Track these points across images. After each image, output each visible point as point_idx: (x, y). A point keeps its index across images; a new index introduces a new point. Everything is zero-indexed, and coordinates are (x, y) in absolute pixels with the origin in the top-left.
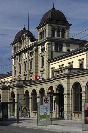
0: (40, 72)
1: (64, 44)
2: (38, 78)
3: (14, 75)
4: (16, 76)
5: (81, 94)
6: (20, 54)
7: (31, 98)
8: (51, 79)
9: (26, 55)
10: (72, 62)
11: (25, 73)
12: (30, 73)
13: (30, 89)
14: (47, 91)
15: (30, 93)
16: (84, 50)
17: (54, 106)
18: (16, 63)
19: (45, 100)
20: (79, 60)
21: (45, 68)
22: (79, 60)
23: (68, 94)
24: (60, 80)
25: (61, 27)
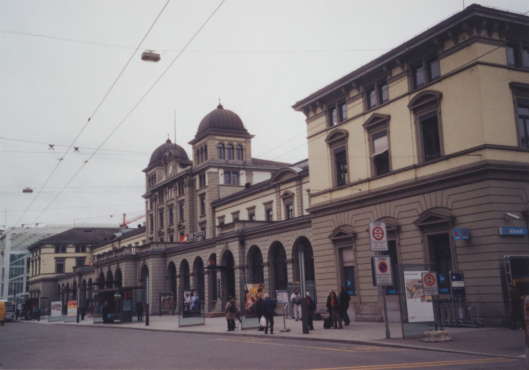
0: (198, 225)
1: (241, 172)
4: (154, 233)
5: (234, 270)
8: (209, 241)
9: (172, 194)
10: (254, 208)
11: (181, 223)
13: (177, 260)
14: (206, 263)
15: (178, 267)
16: (272, 186)
17: (219, 289)
18: (154, 208)
19: (427, 281)
20: (265, 204)
21: (208, 217)
22: (265, 204)
23: (242, 268)
25: (235, 141)
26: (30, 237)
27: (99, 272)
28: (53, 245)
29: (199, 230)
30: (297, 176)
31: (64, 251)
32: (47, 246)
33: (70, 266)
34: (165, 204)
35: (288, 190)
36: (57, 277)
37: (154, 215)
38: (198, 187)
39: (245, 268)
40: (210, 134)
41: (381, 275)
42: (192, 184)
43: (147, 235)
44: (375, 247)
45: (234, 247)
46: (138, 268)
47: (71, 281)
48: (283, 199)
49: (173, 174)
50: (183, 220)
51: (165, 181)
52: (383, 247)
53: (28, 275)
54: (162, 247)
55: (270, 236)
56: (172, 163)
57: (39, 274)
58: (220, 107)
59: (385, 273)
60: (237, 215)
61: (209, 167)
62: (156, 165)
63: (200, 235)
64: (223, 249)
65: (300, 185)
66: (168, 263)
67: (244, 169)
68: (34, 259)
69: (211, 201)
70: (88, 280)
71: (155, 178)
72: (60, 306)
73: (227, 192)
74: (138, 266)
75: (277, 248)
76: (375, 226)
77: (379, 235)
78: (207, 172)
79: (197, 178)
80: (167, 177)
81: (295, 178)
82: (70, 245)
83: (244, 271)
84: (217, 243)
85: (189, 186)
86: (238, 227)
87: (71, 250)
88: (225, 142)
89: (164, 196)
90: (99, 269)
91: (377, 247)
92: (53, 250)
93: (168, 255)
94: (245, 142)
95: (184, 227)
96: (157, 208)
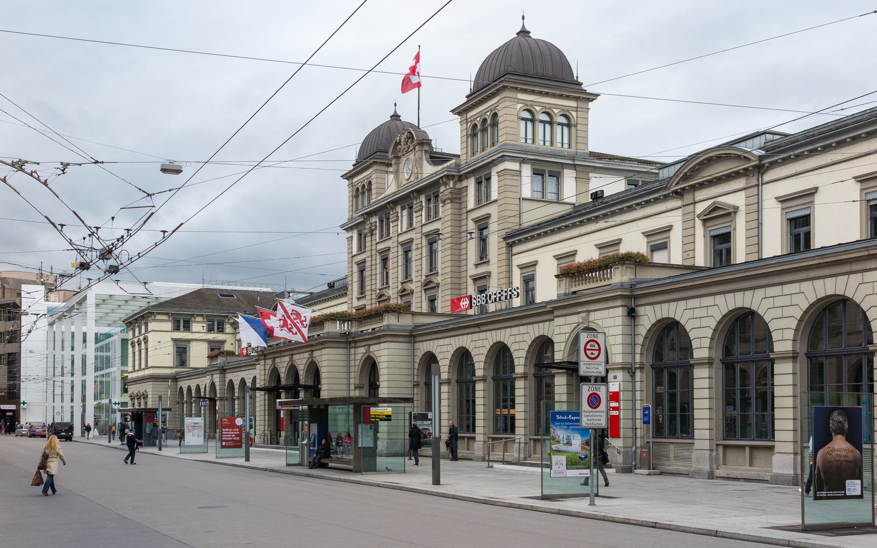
0: (470, 281)
2: (465, 303)
3: (356, 294)
4: (368, 297)
6: (384, 211)
7: (525, 376)
10: (534, 264)
11: (406, 286)
12: (426, 285)
20: (648, 235)
21: (494, 267)
22: (558, 258)
24: (589, 312)
26: (126, 301)
27: (268, 367)
28: (169, 317)
29: (471, 290)
30: (753, 166)
31: (187, 328)
32: (158, 317)
33: (198, 356)
34: (395, 239)
35: (720, 199)
36: (177, 373)
37: (368, 264)
38: (471, 204)
39: (636, 368)
40: (376, 162)
41: (590, 412)
42: (458, 197)
43: (350, 302)
44: (585, 370)
45: (217, 378)
46: (352, 363)
47: (204, 382)
48: (705, 221)
49: (412, 179)
50: (409, 279)
51: (395, 193)
52: (598, 370)
53: (124, 368)
54: (407, 321)
55: (452, 339)
56: (412, 156)
57: (147, 367)
58: (524, 32)
59: (597, 409)
60: (532, 269)
61: (502, 159)
62: (374, 162)
63: (503, 298)
64: (573, 326)
65: (758, 185)
66: (227, 380)
67: (574, 167)
68: (136, 340)
69: (503, 233)
70: (238, 382)
71: (370, 190)
72: (201, 427)
73: (534, 215)
74: (352, 357)
75: (500, 353)
76: (590, 339)
77: (594, 352)
78: (494, 171)
79: (471, 184)
80: (398, 186)
81: (746, 170)
82: (199, 319)
83: (633, 375)
84: (556, 313)
85: (452, 201)
86: (622, 276)
87: (198, 327)
88: (536, 107)
89: (391, 225)
90: (269, 362)
91: (588, 370)
92: (169, 326)
93: (179, 380)
94: (577, 109)
95: (412, 292)
96: (374, 247)
